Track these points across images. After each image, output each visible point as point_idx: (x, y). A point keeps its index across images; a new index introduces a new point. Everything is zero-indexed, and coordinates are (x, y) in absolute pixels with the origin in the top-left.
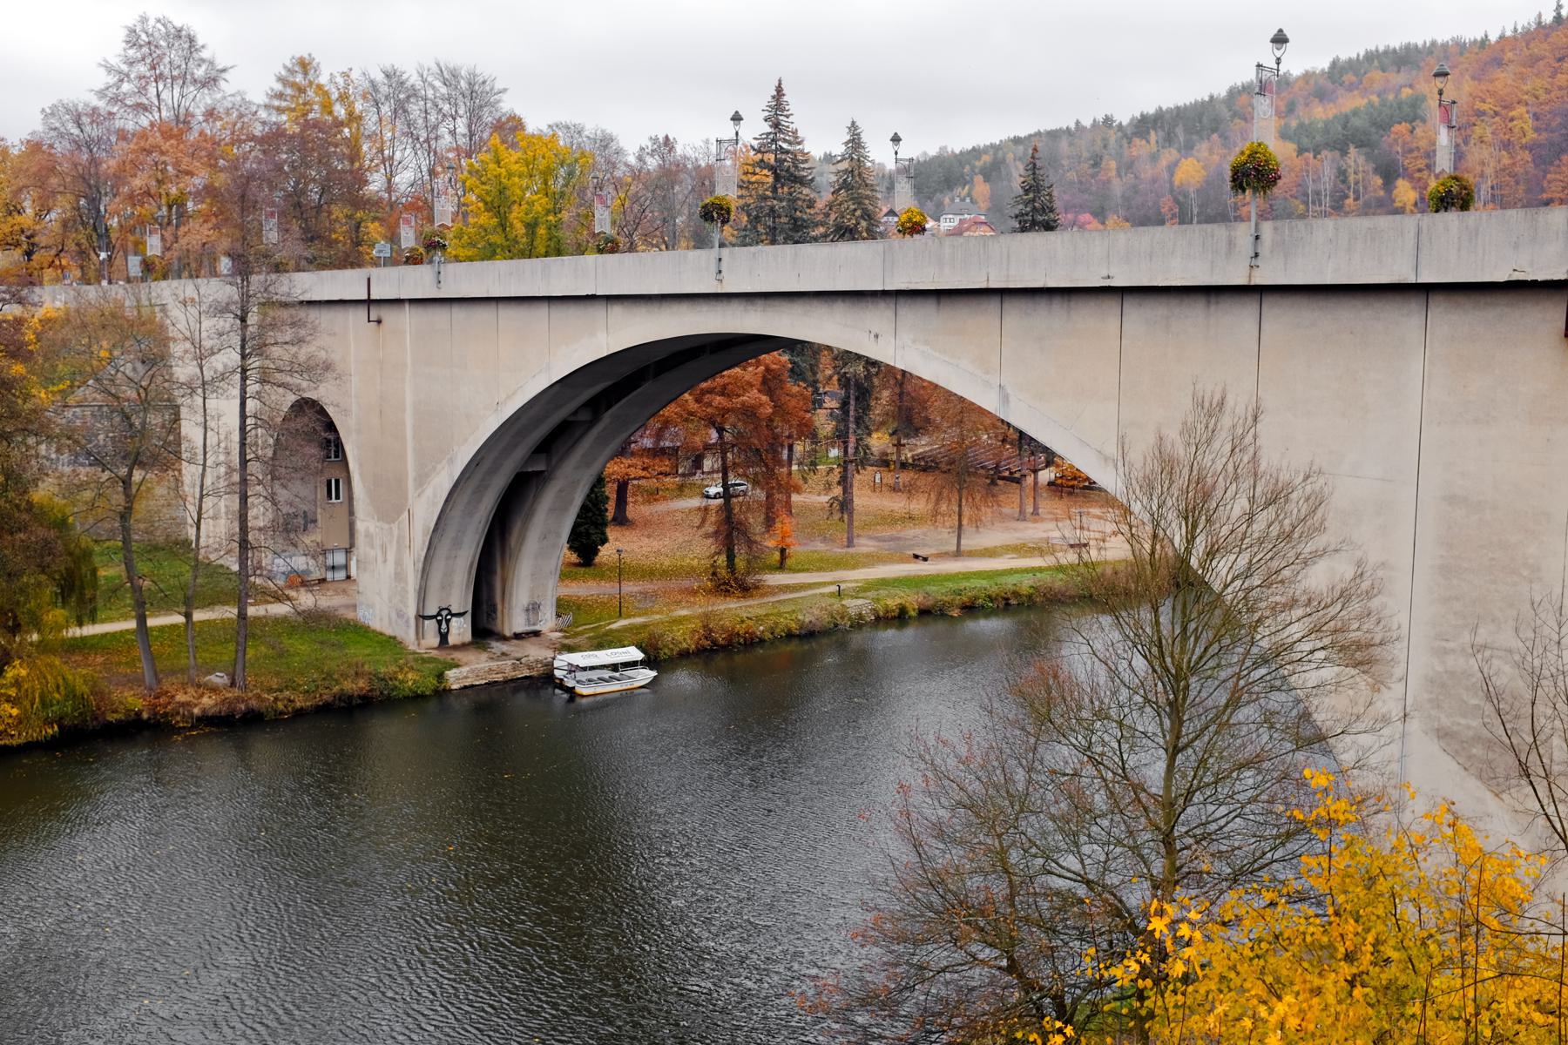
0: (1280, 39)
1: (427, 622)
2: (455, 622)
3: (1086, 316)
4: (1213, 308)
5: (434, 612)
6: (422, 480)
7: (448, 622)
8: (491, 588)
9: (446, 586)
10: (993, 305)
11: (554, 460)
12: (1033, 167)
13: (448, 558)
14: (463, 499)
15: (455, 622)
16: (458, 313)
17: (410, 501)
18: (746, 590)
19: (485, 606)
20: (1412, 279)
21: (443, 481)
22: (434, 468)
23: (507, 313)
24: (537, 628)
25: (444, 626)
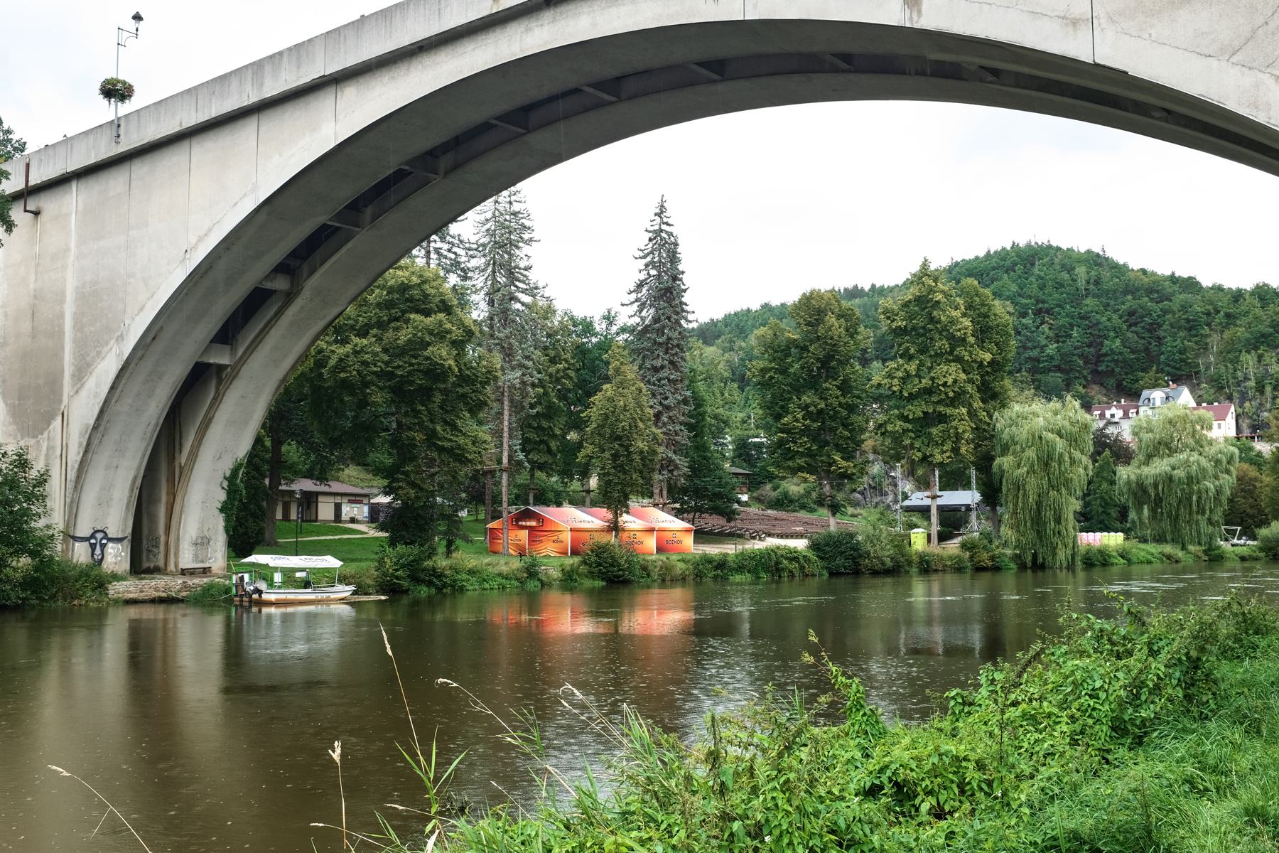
1: (77, 544)
2: (111, 549)
5: (87, 533)
6: (81, 373)
7: (103, 546)
8: (153, 519)
9: (104, 502)
11: (240, 352)
12: (529, 228)
13: (108, 468)
14: (134, 385)
15: (111, 549)
17: (65, 401)
18: (286, 647)
19: (145, 542)
21: (108, 368)
22: (99, 353)
25: (98, 551)
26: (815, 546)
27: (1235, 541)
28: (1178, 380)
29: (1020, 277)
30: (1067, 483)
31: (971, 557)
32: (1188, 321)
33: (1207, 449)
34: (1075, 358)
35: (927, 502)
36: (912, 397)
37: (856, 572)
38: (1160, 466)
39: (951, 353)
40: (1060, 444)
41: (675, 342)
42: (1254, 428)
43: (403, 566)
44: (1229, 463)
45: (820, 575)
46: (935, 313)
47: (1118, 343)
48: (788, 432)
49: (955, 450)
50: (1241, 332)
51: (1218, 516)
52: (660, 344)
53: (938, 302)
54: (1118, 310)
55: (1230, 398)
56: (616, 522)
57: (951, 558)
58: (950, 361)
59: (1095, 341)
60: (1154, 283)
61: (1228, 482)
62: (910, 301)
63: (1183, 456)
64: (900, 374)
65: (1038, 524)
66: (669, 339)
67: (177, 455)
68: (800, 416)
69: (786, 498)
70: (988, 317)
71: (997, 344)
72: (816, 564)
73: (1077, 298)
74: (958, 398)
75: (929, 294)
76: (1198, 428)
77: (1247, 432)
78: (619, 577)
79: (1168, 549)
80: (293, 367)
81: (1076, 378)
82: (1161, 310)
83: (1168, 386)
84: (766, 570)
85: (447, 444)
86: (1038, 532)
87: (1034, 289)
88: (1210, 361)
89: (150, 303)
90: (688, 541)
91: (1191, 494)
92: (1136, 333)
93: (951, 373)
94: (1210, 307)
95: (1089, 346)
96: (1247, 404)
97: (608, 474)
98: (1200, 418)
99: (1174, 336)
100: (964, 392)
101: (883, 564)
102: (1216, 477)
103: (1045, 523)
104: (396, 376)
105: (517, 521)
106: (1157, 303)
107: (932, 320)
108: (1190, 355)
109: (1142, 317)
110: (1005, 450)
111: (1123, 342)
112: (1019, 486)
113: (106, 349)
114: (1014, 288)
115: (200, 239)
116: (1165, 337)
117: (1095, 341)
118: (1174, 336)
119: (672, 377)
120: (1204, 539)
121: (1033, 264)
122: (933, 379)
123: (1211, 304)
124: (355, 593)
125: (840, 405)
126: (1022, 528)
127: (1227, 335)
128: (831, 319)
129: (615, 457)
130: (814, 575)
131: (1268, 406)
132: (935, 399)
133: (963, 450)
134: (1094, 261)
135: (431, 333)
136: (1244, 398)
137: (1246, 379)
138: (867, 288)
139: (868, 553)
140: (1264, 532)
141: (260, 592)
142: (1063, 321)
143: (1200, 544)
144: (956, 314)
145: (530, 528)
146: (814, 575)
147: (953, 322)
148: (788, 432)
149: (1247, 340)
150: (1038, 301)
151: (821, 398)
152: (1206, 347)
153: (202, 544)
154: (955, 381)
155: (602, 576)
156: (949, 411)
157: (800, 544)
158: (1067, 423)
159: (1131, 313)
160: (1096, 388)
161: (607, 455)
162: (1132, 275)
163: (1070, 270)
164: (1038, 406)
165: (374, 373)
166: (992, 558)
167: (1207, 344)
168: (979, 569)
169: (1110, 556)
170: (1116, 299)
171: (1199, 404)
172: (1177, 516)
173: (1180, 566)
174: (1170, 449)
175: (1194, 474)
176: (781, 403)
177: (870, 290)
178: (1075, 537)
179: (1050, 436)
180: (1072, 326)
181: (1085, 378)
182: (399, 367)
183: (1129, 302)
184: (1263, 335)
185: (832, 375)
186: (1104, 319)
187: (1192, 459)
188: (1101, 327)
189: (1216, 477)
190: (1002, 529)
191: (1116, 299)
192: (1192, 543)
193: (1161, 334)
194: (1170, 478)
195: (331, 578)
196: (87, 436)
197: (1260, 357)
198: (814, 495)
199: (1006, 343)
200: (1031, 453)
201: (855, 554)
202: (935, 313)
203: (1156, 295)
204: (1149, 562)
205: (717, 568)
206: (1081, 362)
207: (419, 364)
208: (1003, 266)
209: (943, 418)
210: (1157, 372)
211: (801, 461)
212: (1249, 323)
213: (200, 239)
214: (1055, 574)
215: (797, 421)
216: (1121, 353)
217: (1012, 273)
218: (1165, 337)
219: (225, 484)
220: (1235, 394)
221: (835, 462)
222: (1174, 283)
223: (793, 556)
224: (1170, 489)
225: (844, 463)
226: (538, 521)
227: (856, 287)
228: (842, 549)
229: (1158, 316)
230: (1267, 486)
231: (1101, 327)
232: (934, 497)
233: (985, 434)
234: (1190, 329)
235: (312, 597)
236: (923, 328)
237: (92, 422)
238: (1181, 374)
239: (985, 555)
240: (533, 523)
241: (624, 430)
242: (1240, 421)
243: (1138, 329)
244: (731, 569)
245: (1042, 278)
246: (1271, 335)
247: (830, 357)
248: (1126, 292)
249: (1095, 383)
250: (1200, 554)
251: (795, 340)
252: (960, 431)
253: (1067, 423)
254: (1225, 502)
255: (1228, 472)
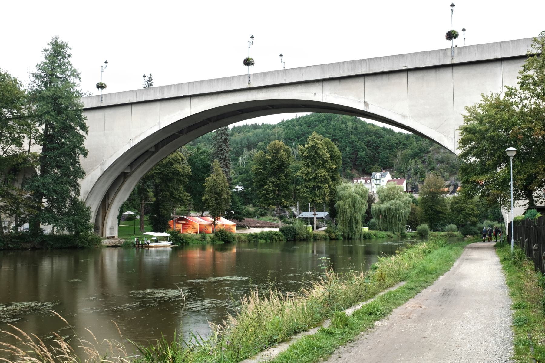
0: (464, 30)
3: (395, 79)
4: (437, 72)
10: (362, 79)
11: (134, 169)
14: (103, 179)
16: (108, 112)
20: (500, 57)
23: (136, 109)
24: (113, 236)
26: (281, 230)
27: (408, 231)
28: (385, 168)
29: (326, 125)
30: (360, 211)
31: (329, 235)
32: (390, 146)
33: (402, 199)
34: (347, 159)
35: (313, 216)
36: (309, 180)
37: (295, 240)
38: (386, 205)
39: (323, 165)
40: (359, 197)
41: (228, 158)
42: (412, 188)
43: (173, 236)
44: (409, 204)
45: (284, 241)
46: (318, 151)
47: (363, 153)
48: (267, 191)
49: (324, 199)
50: (409, 151)
51: (405, 222)
52: (222, 158)
53: (319, 148)
54: (364, 141)
55: (404, 177)
56: (215, 222)
57: (323, 235)
58: (323, 168)
59: (355, 152)
60: (377, 130)
61: (408, 210)
62: (309, 147)
63: (394, 201)
64: (306, 172)
65: (350, 224)
66: (226, 157)
67: (107, 200)
68: (271, 186)
69: (248, 213)
70: (333, 152)
71: (336, 161)
72: (283, 237)
73: (348, 135)
74: (325, 181)
75: (316, 145)
76: (399, 191)
77: (410, 190)
78: (227, 240)
79: (389, 233)
80: (146, 173)
81: (347, 167)
82: (380, 141)
83: (382, 171)
84: (269, 239)
85: (177, 196)
86: (350, 227)
87: (331, 131)
88: (397, 162)
89: (115, 155)
90: (234, 229)
91: (396, 214)
92: (370, 150)
93: (323, 172)
94: (397, 141)
95: (353, 154)
96: (410, 179)
97: (214, 206)
98: (400, 188)
99: (384, 151)
100: (327, 179)
101: (303, 237)
102: (405, 209)
103: (352, 224)
104: (163, 174)
105: (178, 221)
106: (378, 138)
107: (316, 153)
108: (390, 159)
109: (372, 144)
110: (340, 199)
111: (365, 153)
112: (344, 211)
113: (95, 167)
114: (324, 130)
115: (136, 137)
116: (381, 152)
117: (355, 152)
118: (384, 151)
119: (226, 170)
120: (400, 230)
121: (331, 120)
122: (316, 174)
123: (398, 140)
124: (172, 244)
125: (285, 182)
126: (345, 226)
127: (404, 152)
128: (282, 152)
129: (216, 200)
130: (282, 241)
131: (418, 180)
132: (317, 181)
133: (326, 199)
134: (355, 120)
135: (174, 160)
136: (409, 177)
137: (410, 169)
138: (260, 124)
139: (299, 234)
140: (419, 227)
141: (148, 243)
142: (343, 144)
143: (398, 232)
144: (325, 152)
145: (183, 224)
146: (282, 241)
147: (324, 154)
148: (267, 191)
149: (411, 154)
150: (333, 136)
151: (278, 179)
152: (396, 156)
153: (112, 229)
154: (324, 175)
155: (223, 240)
156: (322, 185)
157: (277, 230)
158: (360, 190)
159: (369, 142)
160: (355, 171)
161: (213, 199)
162: (369, 126)
163: (346, 123)
164: (350, 184)
165: (156, 173)
166: (336, 236)
167: (396, 155)
168: (332, 239)
169: (371, 235)
170: (363, 136)
171: (393, 178)
172: (392, 222)
173: (393, 239)
174: (389, 198)
175: (397, 207)
176: (264, 181)
177: (262, 125)
178: (362, 229)
179: (355, 194)
180: (346, 146)
181: (351, 167)
182: (163, 171)
183: (368, 138)
184: (417, 153)
185: (282, 171)
186: (359, 144)
187: (397, 202)
188: (357, 147)
189: (405, 209)
190: (338, 226)
191: (363, 136)
192: (396, 231)
193: (379, 151)
194: (390, 209)
195: (166, 239)
196: (87, 195)
197: (416, 161)
198: (259, 212)
199: (339, 161)
200: (349, 200)
201: (295, 234)
202: (318, 151)
203: (378, 135)
204: (383, 238)
205: (254, 238)
206: (349, 161)
207: (171, 170)
208: (319, 120)
209: (319, 187)
210: (378, 165)
211: (271, 201)
212: (412, 148)
213: (136, 137)
214: (355, 241)
215: (270, 187)
216: (365, 158)
217: (323, 123)
218: (381, 152)
219: (120, 209)
220: (406, 175)
221: (283, 202)
222: (384, 130)
223: (276, 234)
224: (390, 213)
225: (285, 202)
226: (186, 221)
227: (256, 124)
228: (291, 232)
229: (379, 144)
230: (419, 211)
231: (357, 147)
232: (315, 215)
233: (333, 193)
234: (390, 149)
235: (162, 245)
236: (313, 156)
237: (90, 190)
238: (386, 166)
239: (333, 235)
240: (184, 222)
241: (220, 191)
242: (408, 185)
243: (371, 148)
244: (259, 238)
245: (335, 126)
246: (419, 153)
247: (281, 165)
248: (367, 134)
249: (354, 169)
250: (399, 235)
251: (269, 159)
252: (326, 192)
253: (360, 190)
254: (407, 217)
255: (408, 207)
